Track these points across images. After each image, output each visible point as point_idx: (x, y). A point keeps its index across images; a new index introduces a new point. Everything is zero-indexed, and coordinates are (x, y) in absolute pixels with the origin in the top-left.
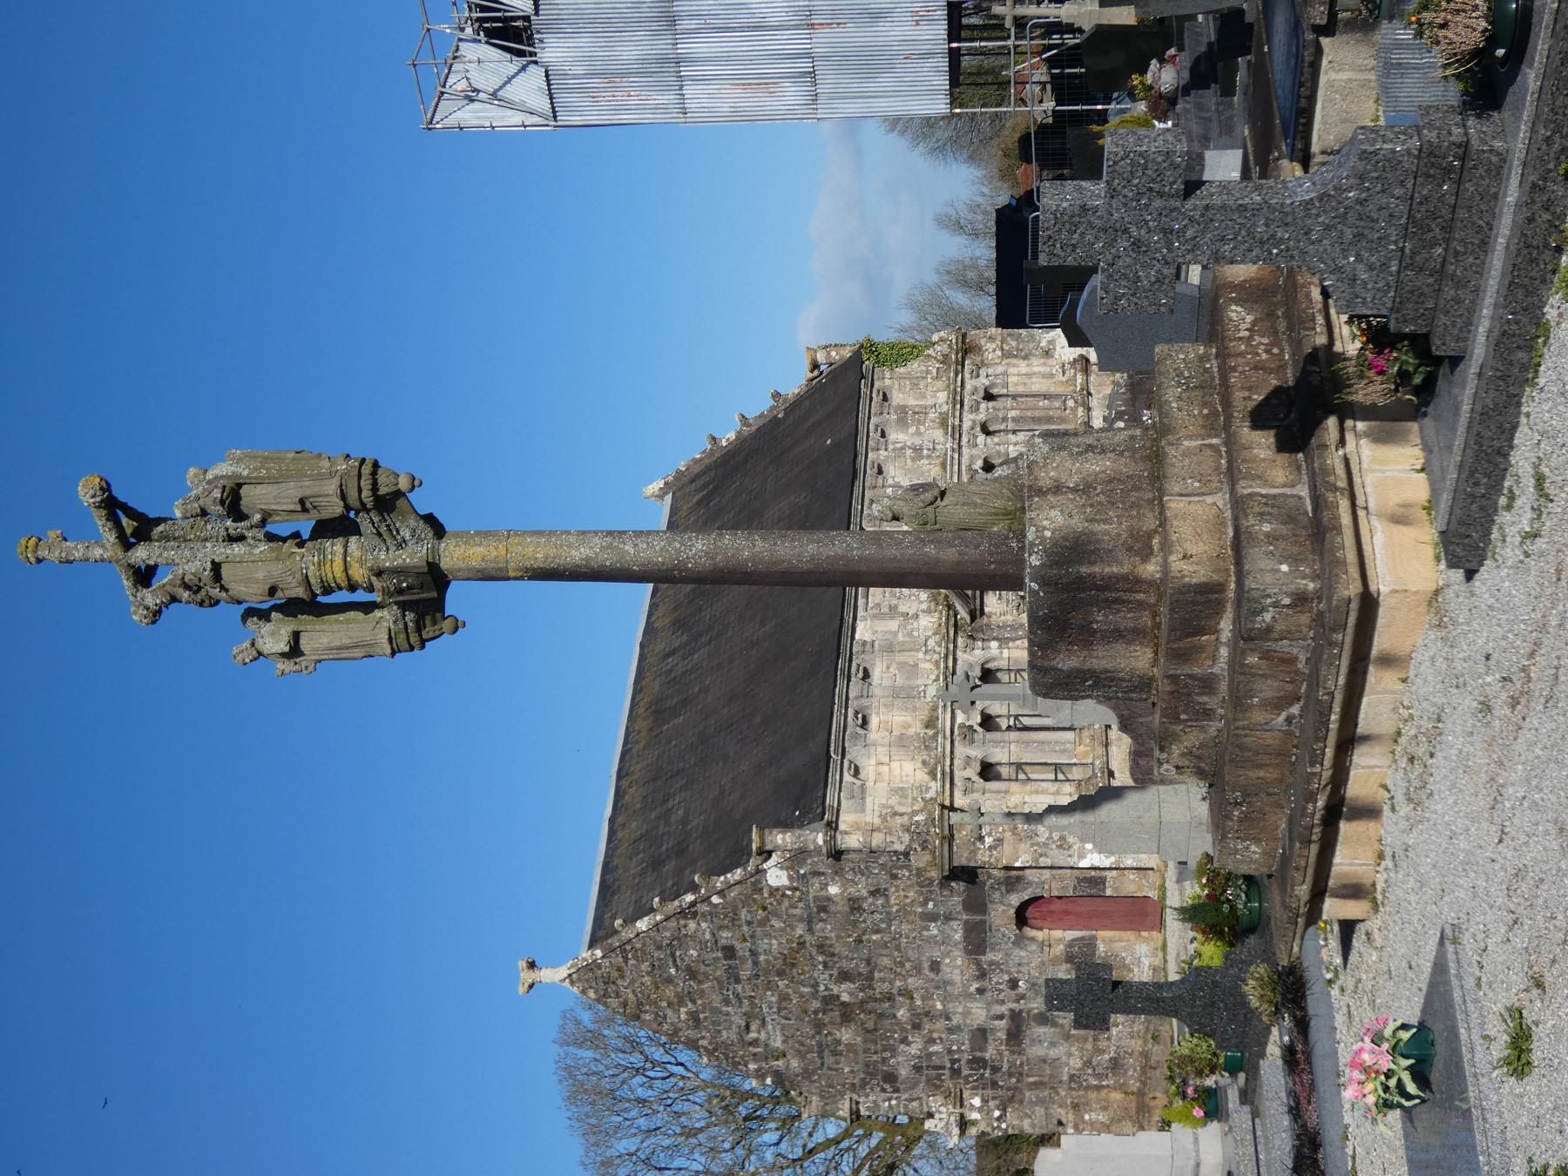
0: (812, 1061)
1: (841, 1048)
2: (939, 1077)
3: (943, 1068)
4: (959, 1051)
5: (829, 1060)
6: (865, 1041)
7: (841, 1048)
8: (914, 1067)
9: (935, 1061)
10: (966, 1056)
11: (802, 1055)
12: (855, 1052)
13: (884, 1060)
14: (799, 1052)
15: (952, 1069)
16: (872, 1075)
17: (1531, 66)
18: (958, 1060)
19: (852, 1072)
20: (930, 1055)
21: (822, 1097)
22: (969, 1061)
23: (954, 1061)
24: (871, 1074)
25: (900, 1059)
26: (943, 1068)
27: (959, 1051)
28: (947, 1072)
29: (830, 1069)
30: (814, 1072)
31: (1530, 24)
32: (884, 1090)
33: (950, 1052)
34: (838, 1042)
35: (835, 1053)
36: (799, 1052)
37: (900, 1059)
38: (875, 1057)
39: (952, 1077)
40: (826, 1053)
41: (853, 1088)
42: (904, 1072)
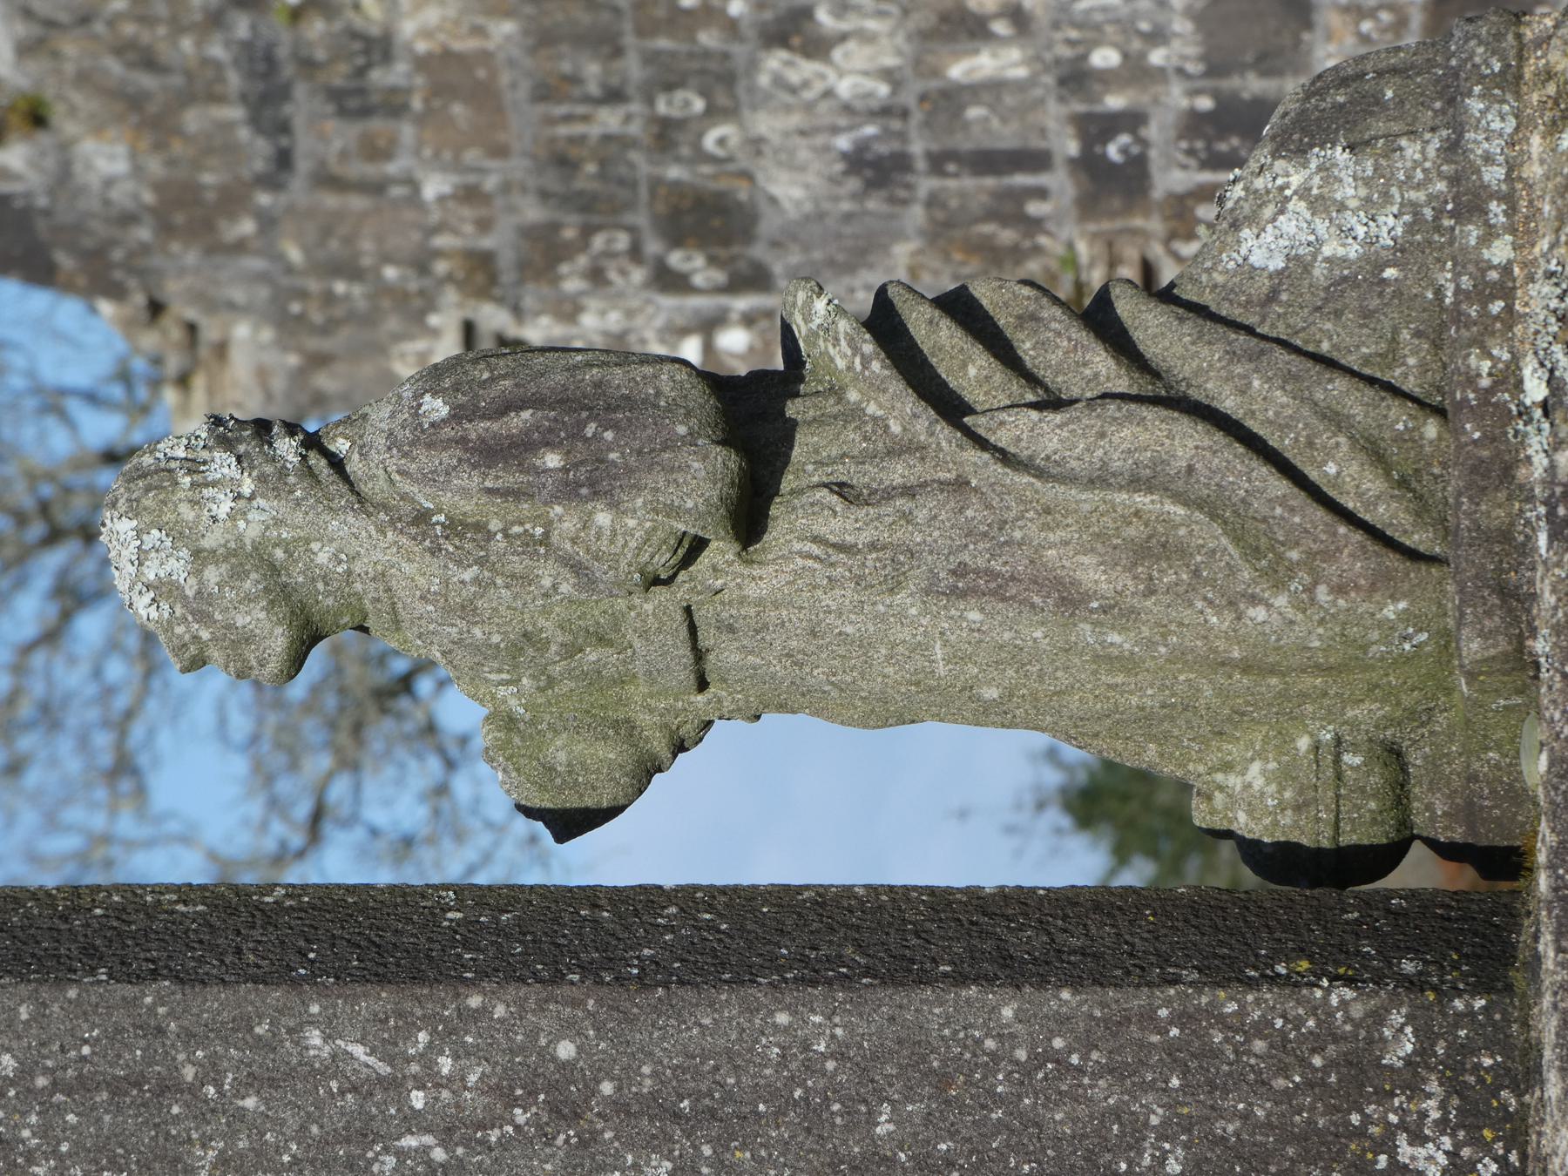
0: (219, 145)
1: (397, 74)
2: (1010, 209)
3: (1038, 160)
4: (1136, 71)
5: (323, 137)
6: (543, 39)
7: (397, 74)
8: (857, 161)
9: (984, 125)
10: (1177, 97)
11: (150, 120)
12: (485, 96)
13: (666, 134)
14: (135, 102)
15: (1090, 165)
16: (596, 210)
17: (994, 55)
18: (1132, 120)
19: (470, 194)
20: (951, 100)
21: (288, 326)
22: (1194, 124)
23: (1096, 129)
24: (585, 203)
25: (765, 124)
26: (1038, 160)
27: (1136, 71)
28: (1059, 182)
29: (327, 180)
30: (233, 200)
31: (996, 356)
32: (668, 281)
33: (1076, 78)
34: (380, 47)
35: (352, 102)
36: (135, 102)
37: (765, 124)
38: (609, 120)
39: (1088, 206)
40: (303, 106)
41: (481, 274)
42: (789, 190)
